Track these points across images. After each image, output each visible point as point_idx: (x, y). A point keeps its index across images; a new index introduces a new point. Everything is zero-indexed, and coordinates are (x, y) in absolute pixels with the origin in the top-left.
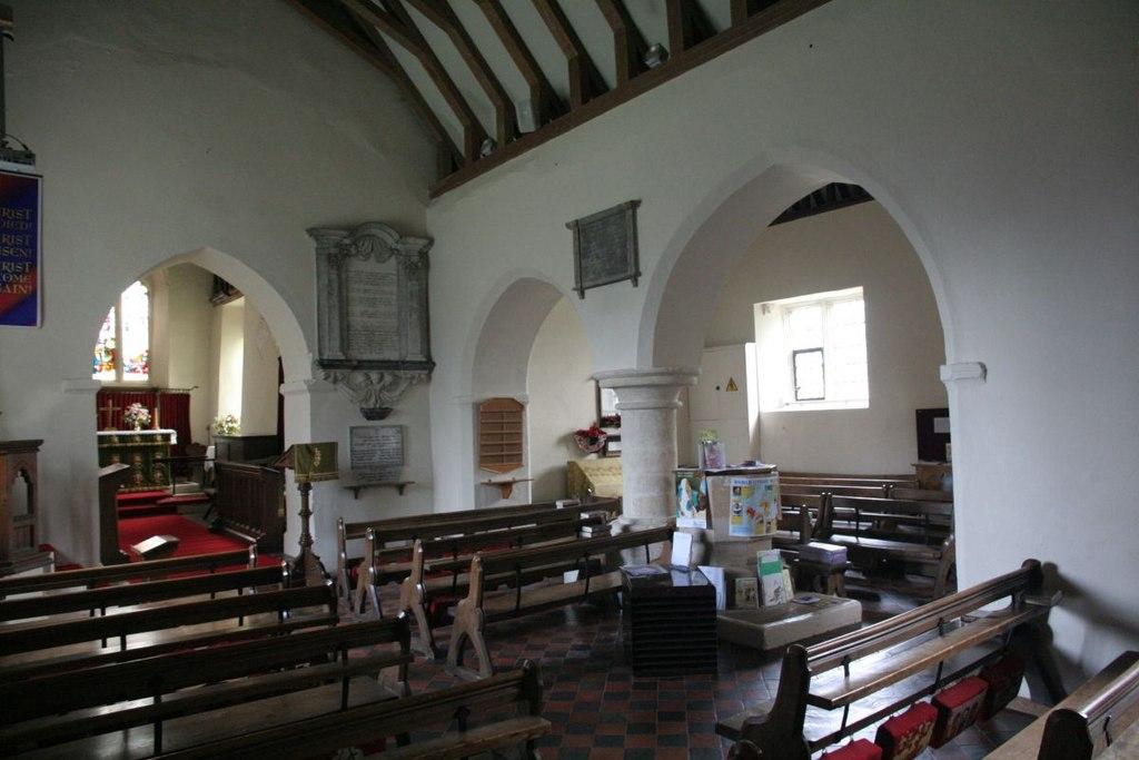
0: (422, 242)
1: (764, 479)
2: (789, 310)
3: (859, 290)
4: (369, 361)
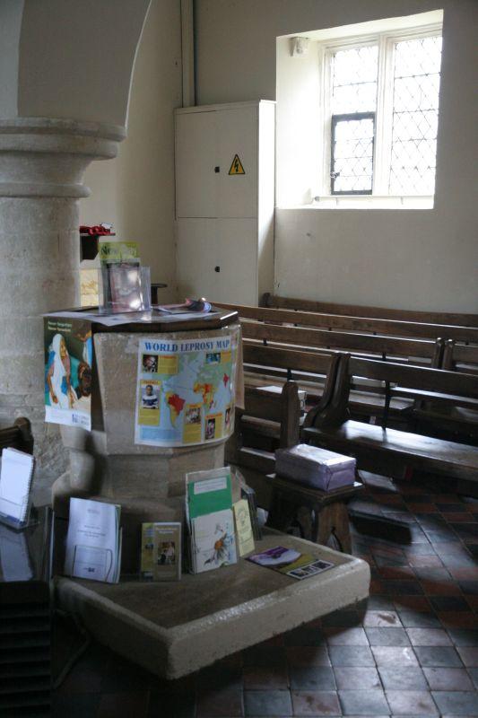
1: (205, 341)
2: (330, 50)
3: (436, 17)
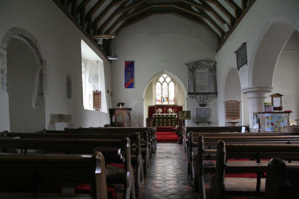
0: (213, 64)
1: (277, 115)
4: (200, 93)
